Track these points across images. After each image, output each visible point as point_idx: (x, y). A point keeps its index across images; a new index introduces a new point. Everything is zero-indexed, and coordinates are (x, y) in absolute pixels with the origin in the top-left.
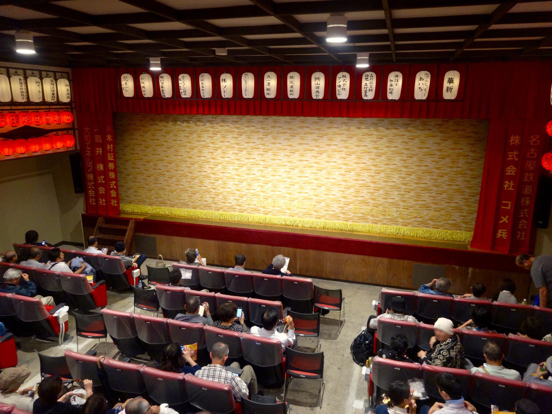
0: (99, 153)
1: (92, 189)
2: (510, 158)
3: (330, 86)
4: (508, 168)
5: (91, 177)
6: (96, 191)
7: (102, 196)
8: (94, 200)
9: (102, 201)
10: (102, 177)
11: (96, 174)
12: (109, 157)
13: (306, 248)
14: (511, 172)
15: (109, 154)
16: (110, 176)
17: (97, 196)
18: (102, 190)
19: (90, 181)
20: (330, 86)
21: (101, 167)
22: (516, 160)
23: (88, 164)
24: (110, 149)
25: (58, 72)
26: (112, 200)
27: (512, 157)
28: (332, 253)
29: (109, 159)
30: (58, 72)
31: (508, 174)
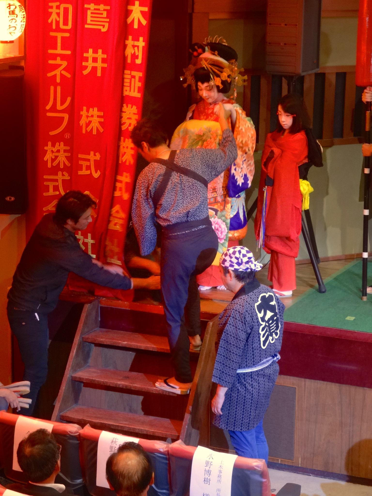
0: (94, 69)
5: (54, 154)
11: (76, 140)
19: (55, 170)
22: (96, 175)
23: (54, 109)
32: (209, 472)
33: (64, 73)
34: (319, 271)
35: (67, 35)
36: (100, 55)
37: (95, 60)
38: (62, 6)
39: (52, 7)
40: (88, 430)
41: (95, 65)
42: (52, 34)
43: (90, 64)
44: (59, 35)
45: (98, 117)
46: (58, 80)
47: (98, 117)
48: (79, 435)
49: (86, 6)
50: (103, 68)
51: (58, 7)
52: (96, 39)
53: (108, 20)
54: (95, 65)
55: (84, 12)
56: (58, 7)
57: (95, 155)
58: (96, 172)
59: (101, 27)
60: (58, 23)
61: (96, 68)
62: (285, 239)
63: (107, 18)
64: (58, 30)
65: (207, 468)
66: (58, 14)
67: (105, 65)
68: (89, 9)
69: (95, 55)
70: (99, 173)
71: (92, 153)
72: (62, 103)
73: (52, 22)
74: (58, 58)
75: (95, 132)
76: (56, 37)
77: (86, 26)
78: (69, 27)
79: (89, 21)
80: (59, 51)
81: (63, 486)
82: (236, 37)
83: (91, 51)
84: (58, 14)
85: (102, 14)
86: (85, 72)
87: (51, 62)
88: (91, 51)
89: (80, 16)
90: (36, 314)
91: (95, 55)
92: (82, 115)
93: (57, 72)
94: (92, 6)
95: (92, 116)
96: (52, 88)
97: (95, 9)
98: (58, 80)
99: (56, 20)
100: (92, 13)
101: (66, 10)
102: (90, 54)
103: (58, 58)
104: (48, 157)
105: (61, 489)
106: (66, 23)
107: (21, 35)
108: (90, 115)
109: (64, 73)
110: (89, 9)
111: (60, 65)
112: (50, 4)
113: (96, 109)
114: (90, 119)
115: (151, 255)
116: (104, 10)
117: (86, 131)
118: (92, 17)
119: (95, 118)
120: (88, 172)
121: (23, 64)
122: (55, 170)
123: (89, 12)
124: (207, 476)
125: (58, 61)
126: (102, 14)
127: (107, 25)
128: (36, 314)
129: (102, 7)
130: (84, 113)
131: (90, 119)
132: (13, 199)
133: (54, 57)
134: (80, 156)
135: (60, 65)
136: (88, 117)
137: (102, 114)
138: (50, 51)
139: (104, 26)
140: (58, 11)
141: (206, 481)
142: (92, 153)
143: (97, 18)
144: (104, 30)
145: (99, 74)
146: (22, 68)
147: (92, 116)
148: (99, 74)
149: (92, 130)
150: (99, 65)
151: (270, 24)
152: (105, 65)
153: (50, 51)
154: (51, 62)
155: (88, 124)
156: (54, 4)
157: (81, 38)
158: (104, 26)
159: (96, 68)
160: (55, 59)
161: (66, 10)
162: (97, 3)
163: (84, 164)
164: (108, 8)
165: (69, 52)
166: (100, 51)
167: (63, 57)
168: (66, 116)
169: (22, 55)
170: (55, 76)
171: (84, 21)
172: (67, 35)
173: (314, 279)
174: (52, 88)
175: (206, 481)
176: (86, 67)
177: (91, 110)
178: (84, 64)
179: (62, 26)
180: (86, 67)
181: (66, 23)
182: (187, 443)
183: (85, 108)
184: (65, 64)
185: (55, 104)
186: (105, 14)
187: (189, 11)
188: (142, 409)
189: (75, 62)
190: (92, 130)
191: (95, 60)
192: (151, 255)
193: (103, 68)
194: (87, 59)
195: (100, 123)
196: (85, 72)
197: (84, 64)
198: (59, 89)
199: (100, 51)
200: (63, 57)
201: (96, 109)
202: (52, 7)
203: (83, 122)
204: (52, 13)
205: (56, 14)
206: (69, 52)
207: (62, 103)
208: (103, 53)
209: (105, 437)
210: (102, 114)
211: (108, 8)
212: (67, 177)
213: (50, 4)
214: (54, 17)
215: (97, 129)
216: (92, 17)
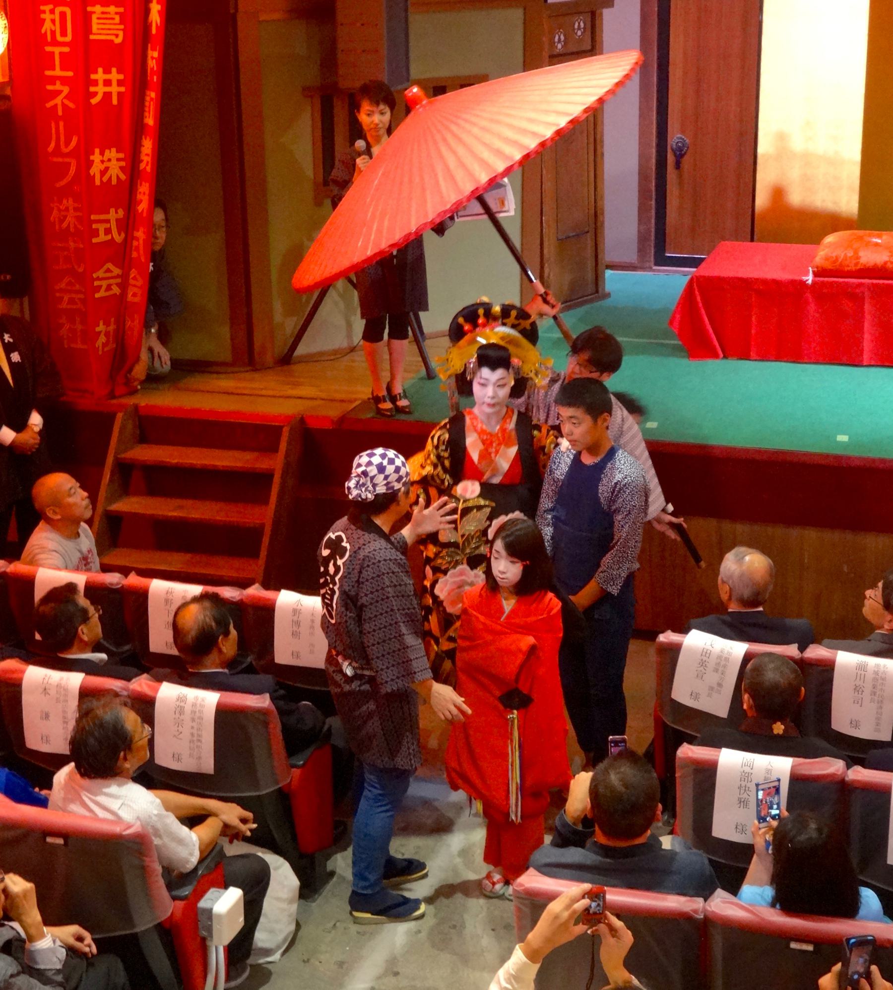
0: (107, 96)
23: (57, 151)
32: (298, 623)
33: (66, 102)
35: (66, 49)
36: (115, 76)
37: (107, 83)
38: (58, 10)
39: (44, 12)
40: (134, 580)
41: (107, 89)
42: (48, 49)
43: (100, 89)
44: (57, 50)
45: (118, 160)
46: (60, 113)
47: (118, 160)
48: (123, 587)
49: (89, 9)
50: (119, 94)
51: (52, 12)
52: (106, 54)
53: (122, 27)
54: (107, 89)
55: (88, 17)
56: (52, 12)
57: (116, 212)
58: (120, 235)
59: (113, 38)
60: (53, 33)
61: (110, 93)
63: (120, 24)
64: (55, 43)
65: (295, 618)
66: (53, 21)
67: (123, 89)
68: (94, 12)
69: (107, 77)
70: (123, 235)
71: (112, 210)
73: (46, 33)
74: (58, 83)
75: (114, 181)
76: (53, 53)
77: (92, 37)
78: (69, 38)
79: (95, 28)
80: (58, 72)
81: (104, 656)
82: (299, 40)
83: (100, 70)
84: (53, 21)
85: (113, 19)
86: (94, 101)
87: (50, 87)
88: (100, 70)
89: (83, 23)
91: (107, 77)
92: (93, 161)
93: (58, 101)
94: (98, 9)
95: (109, 160)
96: (53, 125)
97: (103, 13)
98: (60, 113)
99: (51, 30)
100: (98, 18)
101: (63, 15)
102: (99, 75)
103: (58, 83)
105: (101, 660)
106: (64, 33)
107: (3, 54)
108: (105, 158)
109: (66, 102)
110: (94, 12)
111: (60, 92)
112: (42, 8)
113: (114, 150)
114: (106, 164)
116: (116, 13)
117: (101, 181)
118: (98, 24)
119: (114, 162)
120: (109, 237)
121: (8, 92)
123: (94, 17)
124: (295, 629)
125: (58, 86)
126: (113, 19)
127: (121, 34)
129: (112, 9)
130: (96, 157)
131: (106, 164)
132: (8, 277)
133: (53, 80)
134: (93, 217)
135: (60, 92)
136: (102, 162)
137: (121, 155)
138: (48, 73)
139: (117, 36)
140: (52, 16)
141: (295, 634)
142: (112, 210)
143: (106, 24)
144: (118, 40)
145: (115, 101)
146: (7, 98)
147: (109, 160)
148: (115, 101)
149: (110, 178)
150: (114, 89)
151: (342, 24)
152: (123, 89)
153: (48, 73)
154: (50, 87)
155: (103, 173)
156: (47, 8)
157: (87, 54)
158: (117, 36)
159: (110, 93)
160: (55, 84)
161: (63, 15)
162: (105, 4)
164: (121, 10)
165: (70, 74)
166: (114, 70)
167: (64, 81)
168: (73, 163)
169: (7, 79)
170: (56, 105)
171: (88, 30)
172: (66, 49)
173: (418, 362)
174: (53, 125)
175: (295, 634)
176: (96, 94)
177: (107, 152)
178: (92, 89)
179: (59, 38)
180: (96, 94)
181: (64, 33)
182: (266, 586)
183: (97, 151)
184: (66, 90)
185: (59, 142)
186: (117, 18)
187: (232, 11)
189: (81, 86)
190: (110, 178)
191: (107, 84)
193: (119, 94)
194: (95, 83)
195: (121, 168)
196: (94, 101)
197: (92, 89)
198: (61, 124)
199: (114, 70)
200: (64, 81)
201: (114, 150)
202: (44, 12)
203: (95, 170)
204: (44, 20)
205: (51, 19)
206: (70, 74)
208: (118, 72)
209: (158, 586)
210: (121, 155)
211: (121, 10)
213: (42, 8)
214: (47, 26)
215: (118, 176)
216: (98, 24)
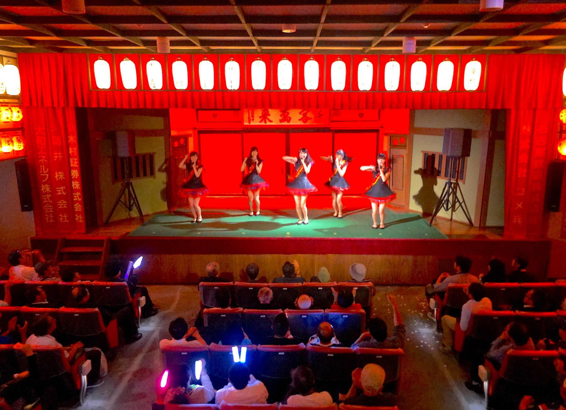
0: (58, 158)
1: (49, 203)
2: (59, 193)
3: (379, 77)
4: (60, 202)
5: (46, 188)
6: (55, 205)
7: (63, 211)
8: (51, 216)
9: (64, 218)
10: (62, 188)
11: (52, 182)
12: (71, 162)
13: (324, 253)
14: (63, 206)
15: (71, 160)
16: (73, 185)
17: (57, 211)
18: (62, 204)
19: (46, 193)
20: (379, 77)
21: (59, 175)
22: (64, 194)
23: (43, 173)
24: (73, 153)
25: (5, 56)
26: (76, 215)
27: (61, 192)
28: (354, 256)
29: (72, 165)
30: (5, 56)
31: (60, 207)
34: (171, 223)
37: (58, 155)
62: (474, 128)
72: (45, 170)
90: (363, 168)
104: (43, 189)
115: (421, 216)
122: (46, 193)
128: (363, 168)
163: (75, 197)
185: (44, 172)
188: (37, 336)
192: (421, 216)
207: (45, 170)
212: (50, 196)
